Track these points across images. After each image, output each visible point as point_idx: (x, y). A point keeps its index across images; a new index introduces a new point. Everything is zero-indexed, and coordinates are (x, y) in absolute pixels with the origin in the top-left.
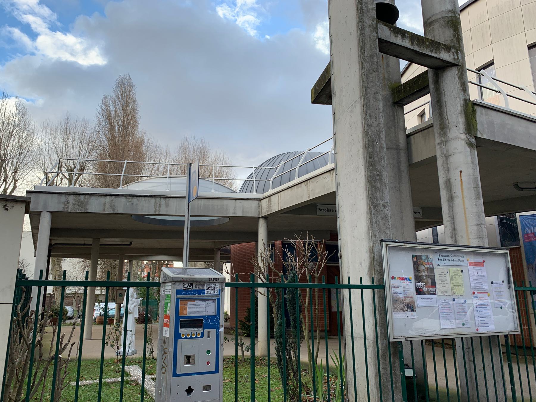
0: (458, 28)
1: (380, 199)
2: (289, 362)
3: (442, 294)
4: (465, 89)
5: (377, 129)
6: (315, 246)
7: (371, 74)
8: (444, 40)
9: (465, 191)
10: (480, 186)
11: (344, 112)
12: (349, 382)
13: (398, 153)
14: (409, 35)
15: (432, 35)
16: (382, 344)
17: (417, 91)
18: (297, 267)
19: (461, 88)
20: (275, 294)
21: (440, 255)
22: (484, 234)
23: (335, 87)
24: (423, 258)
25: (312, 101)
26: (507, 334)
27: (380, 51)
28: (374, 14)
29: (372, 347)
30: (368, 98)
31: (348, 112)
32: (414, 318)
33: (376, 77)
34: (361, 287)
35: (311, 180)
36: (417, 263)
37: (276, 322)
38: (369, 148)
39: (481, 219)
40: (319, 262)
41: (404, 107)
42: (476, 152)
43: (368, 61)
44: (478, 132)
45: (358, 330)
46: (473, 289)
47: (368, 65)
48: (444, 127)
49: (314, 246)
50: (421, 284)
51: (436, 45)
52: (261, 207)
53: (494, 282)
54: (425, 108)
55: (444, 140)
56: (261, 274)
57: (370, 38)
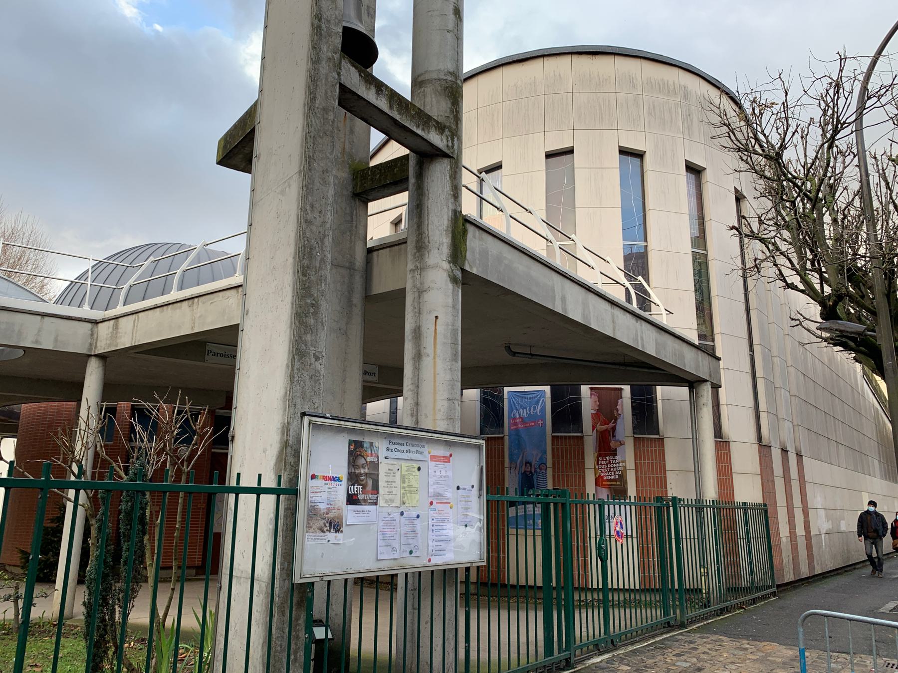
0: (458, 101)
1: (312, 345)
2: (109, 627)
3: (385, 505)
4: (456, 195)
5: (321, 230)
6: (189, 417)
7: (322, 138)
8: (436, 115)
9: (439, 347)
10: (460, 343)
11: (270, 191)
12: (218, 656)
13: (351, 276)
14: (388, 91)
15: (422, 102)
16: (281, 588)
17: (391, 184)
18: (152, 453)
19: (452, 193)
20: (98, 501)
21: (390, 442)
22: (456, 415)
23: (262, 145)
24: (365, 445)
25: (219, 160)
26: (469, 565)
27: (340, 104)
28: (338, 42)
29: (264, 593)
30: (312, 176)
31: (277, 192)
32: (339, 544)
33: (329, 145)
34: (258, 491)
35: (201, 299)
36: (356, 451)
37: (94, 553)
38: (304, 258)
39: (455, 391)
40: (194, 445)
41: (369, 204)
42: (460, 291)
43: (319, 115)
44: (467, 262)
45: (242, 564)
46: (431, 497)
47: (318, 121)
48: (421, 247)
49: (188, 417)
50: (357, 488)
51: (425, 119)
52: (95, 336)
53: (460, 487)
54: (402, 214)
55: (419, 265)
56: (74, 464)
57: (327, 79)
